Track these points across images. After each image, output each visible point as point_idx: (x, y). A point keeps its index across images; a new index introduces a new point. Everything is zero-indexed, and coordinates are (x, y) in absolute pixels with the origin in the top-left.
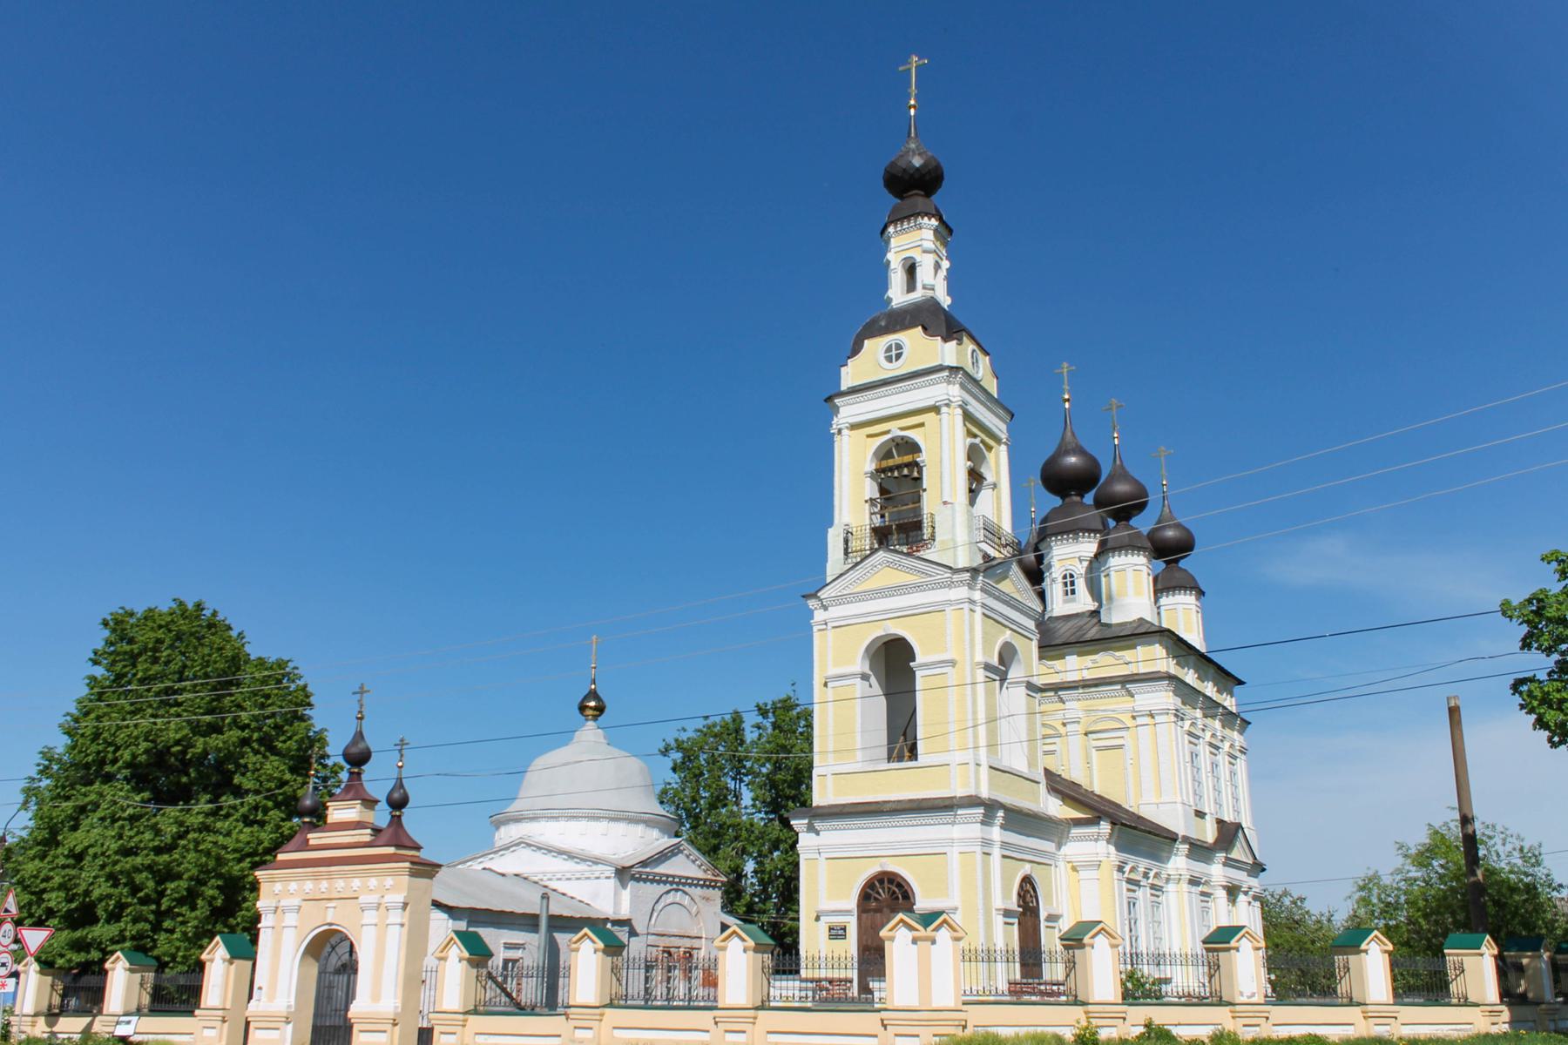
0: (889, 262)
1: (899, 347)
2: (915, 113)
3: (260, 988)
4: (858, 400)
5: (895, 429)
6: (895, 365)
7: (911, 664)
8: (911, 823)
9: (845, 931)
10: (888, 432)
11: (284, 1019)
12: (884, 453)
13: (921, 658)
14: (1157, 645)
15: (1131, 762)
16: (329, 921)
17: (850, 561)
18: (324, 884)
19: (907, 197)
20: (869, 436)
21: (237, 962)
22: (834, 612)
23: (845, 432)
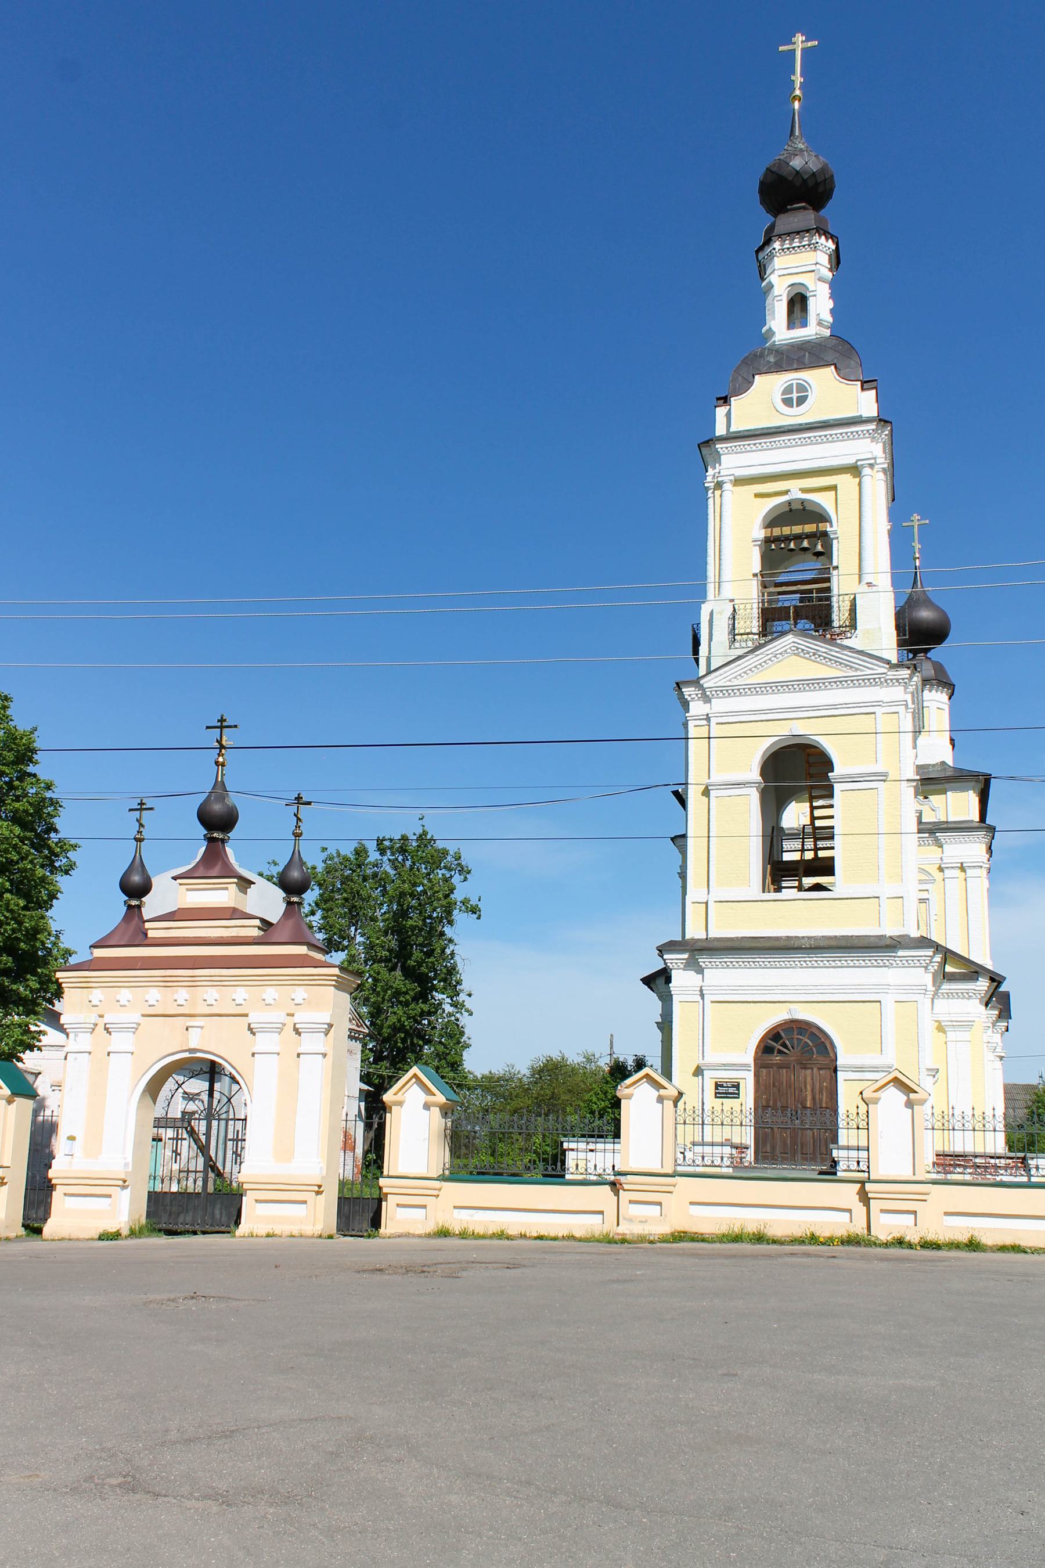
0: (771, 286)
1: (801, 388)
2: (800, 107)
3: (72, 1138)
4: (748, 448)
5: (795, 489)
6: (795, 410)
7: (830, 774)
8: (833, 964)
9: (738, 1089)
10: (787, 492)
11: (121, 1183)
12: (774, 520)
13: (839, 769)
14: (971, 792)
15: (936, 917)
16: (192, 1046)
17: (737, 645)
18: (182, 994)
19: (791, 210)
20: (758, 495)
21: (19, 1100)
22: (719, 705)
23: (727, 486)
